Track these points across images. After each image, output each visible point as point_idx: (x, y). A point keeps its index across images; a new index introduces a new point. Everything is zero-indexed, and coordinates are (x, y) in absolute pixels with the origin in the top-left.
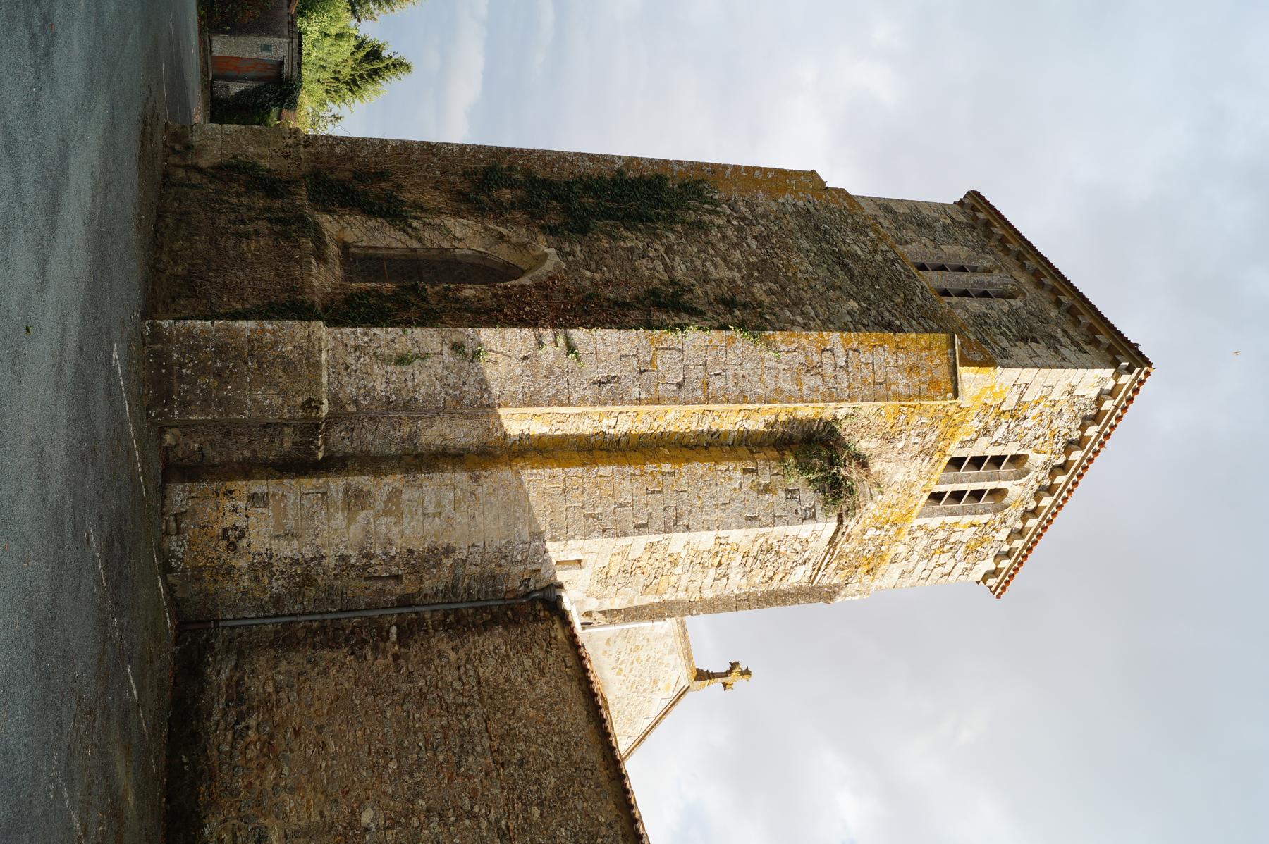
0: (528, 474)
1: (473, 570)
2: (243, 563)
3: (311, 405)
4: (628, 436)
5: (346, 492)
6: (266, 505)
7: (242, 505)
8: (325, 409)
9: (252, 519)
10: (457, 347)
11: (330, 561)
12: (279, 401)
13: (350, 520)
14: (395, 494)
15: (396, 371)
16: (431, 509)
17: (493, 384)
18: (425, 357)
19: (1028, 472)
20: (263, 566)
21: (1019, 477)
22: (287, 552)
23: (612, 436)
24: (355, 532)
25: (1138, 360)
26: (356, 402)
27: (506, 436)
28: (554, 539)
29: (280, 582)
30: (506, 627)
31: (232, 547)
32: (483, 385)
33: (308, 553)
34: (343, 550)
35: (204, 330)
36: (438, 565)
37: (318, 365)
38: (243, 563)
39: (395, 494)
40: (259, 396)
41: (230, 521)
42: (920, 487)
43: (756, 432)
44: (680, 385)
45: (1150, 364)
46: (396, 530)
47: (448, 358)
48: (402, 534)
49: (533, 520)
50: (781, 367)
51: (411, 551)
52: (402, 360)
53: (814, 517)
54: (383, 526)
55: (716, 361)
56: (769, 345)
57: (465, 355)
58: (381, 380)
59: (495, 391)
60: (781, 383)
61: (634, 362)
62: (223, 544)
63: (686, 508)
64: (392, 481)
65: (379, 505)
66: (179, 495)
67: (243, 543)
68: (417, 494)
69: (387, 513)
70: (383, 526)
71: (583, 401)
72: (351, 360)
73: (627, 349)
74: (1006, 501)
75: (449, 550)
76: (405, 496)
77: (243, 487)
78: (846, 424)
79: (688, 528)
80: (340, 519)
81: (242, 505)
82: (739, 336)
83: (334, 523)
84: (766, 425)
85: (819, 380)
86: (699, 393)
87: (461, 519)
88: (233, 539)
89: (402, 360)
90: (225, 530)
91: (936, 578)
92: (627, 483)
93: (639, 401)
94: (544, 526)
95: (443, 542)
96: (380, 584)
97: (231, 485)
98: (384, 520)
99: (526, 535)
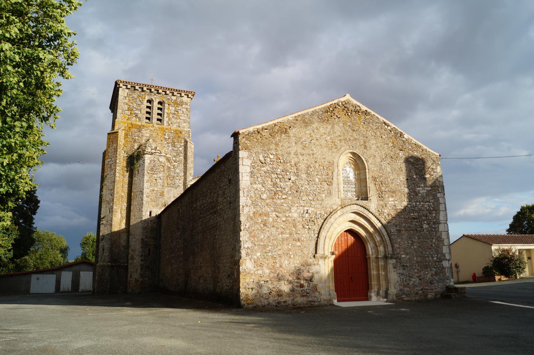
0: (131, 224)
1: (149, 234)
2: (141, 279)
3: (108, 266)
4: (127, 203)
5: (131, 260)
6: (132, 275)
7: (131, 279)
8: (109, 264)
9: (134, 277)
10: (102, 239)
11: (142, 263)
12: (107, 272)
13: (135, 259)
14: (132, 250)
15: (105, 251)
16: (135, 243)
17: (108, 233)
18: (103, 246)
19: (152, 99)
20: (142, 275)
21: (153, 101)
22: (139, 271)
23: (127, 206)
24: (137, 258)
25: (116, 83)
26: (109, 258)
27: (125, 228)
28: (142, 218)
29: (147, 272)
30: (409, 193)
31: (138, 281)
32: (108, 234)
33: (140, 267)
34: (140, 260)
35: (97, 285)
36: (146, 241)
37: (103, 265)
38: (141, 279)
39: (132, 250)
40: (106, 275)
41: (134, 281)
42: (151, 128)
43: (129, 174)
44: (111, 195)
45: (116, 81)
46: (138, 250)
47: (104, 241)
48: (138, 249)
49: (138, 223)
50: (110, 173)
51: (142, 247)
52: (103, 250)
53: (144, 160)
54: (137, 253)
55: (108, 188)
56: (106, 176)
57: (103, 238)
58: (106, 254)
59: (109, 232)
60: (113, 173)
61: (107, 205)
62: (137, 283)
63: (140, 190)
64: (130, 251)
65: (133, 253)
66: (129, 290)
67: (137, 279)
68: (132, 246)
69: (135, 251)
70: (137, 253)
71: (112, 215)
72: (103, 259)
73: (105, 206)
74: (162, 101)
75: (142, 239)
76: (133, 248)
77: (129, 279)
78: (129, 153)
79: (143, 189)
80: (135, 261)
81: (131, 279)
82: (104, 183)
83: (136, 262)
84: (127, 172)
85: (113, 165)
86: (113, 191)
87: (137, 237)
88: (137, 281)
89: (103, 250)
90: (135, 282)
91: (188, 112)
92: (134, 203)
93: (113, 203)
94: (139, 220)
95: (140, 241)
96: (151, 253)
97: (128, 281)
98: (136, 253)
99: (141, 224)
